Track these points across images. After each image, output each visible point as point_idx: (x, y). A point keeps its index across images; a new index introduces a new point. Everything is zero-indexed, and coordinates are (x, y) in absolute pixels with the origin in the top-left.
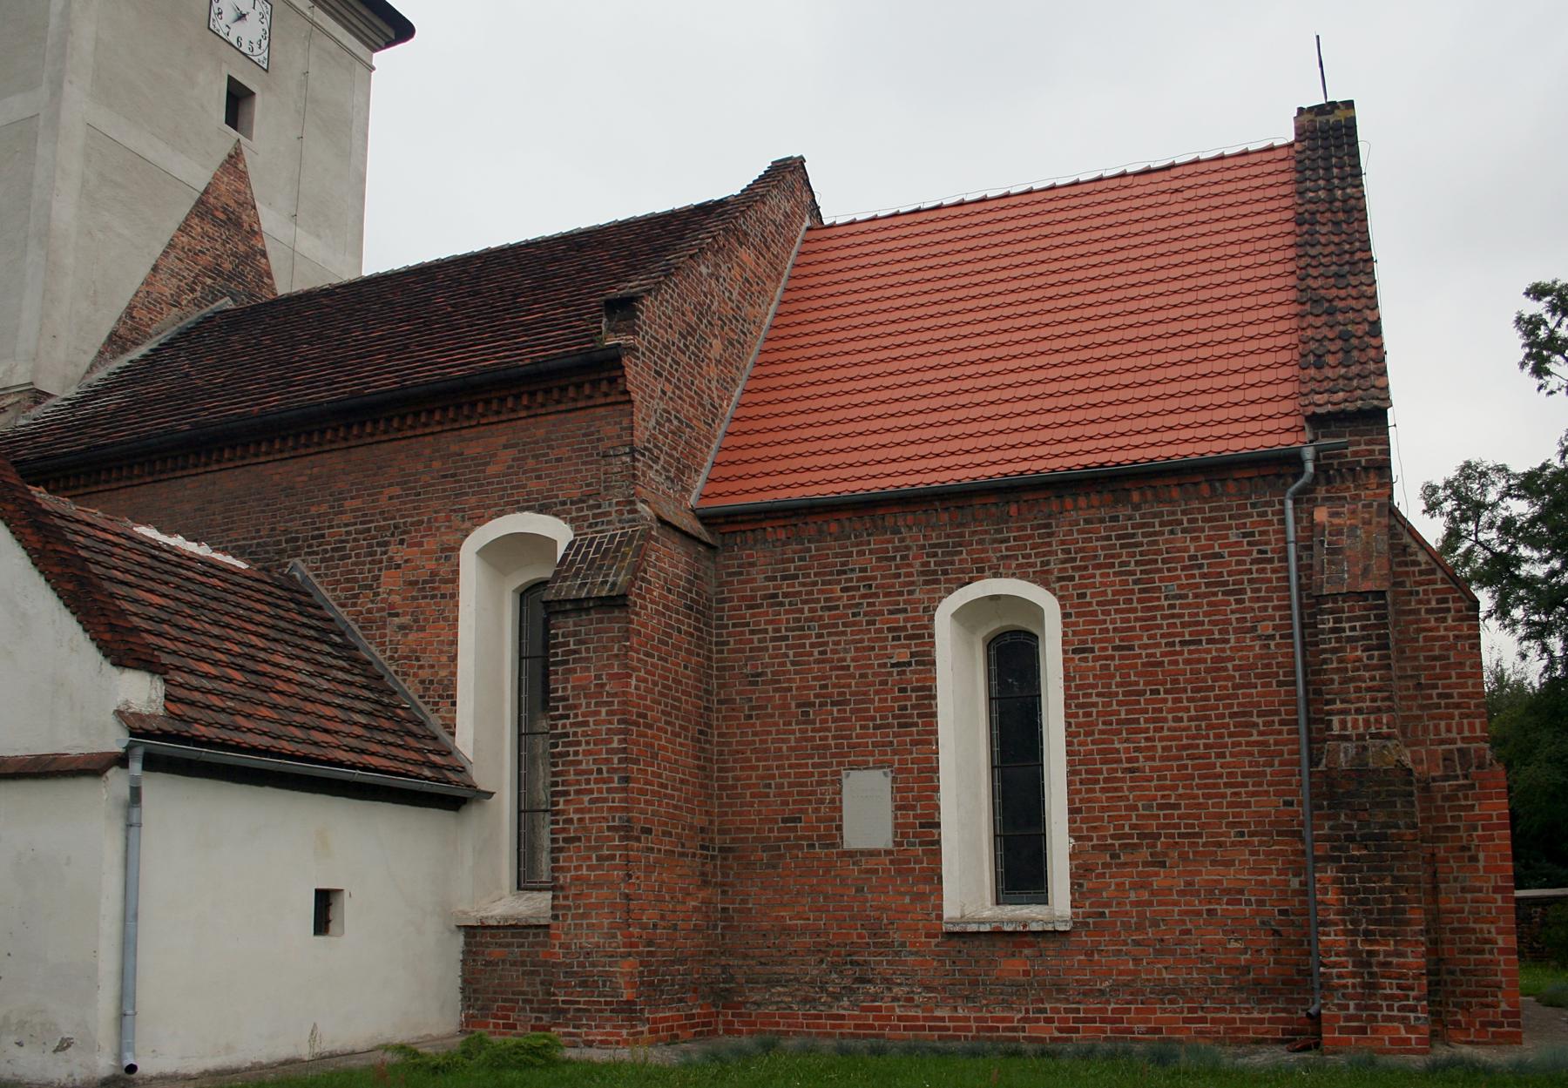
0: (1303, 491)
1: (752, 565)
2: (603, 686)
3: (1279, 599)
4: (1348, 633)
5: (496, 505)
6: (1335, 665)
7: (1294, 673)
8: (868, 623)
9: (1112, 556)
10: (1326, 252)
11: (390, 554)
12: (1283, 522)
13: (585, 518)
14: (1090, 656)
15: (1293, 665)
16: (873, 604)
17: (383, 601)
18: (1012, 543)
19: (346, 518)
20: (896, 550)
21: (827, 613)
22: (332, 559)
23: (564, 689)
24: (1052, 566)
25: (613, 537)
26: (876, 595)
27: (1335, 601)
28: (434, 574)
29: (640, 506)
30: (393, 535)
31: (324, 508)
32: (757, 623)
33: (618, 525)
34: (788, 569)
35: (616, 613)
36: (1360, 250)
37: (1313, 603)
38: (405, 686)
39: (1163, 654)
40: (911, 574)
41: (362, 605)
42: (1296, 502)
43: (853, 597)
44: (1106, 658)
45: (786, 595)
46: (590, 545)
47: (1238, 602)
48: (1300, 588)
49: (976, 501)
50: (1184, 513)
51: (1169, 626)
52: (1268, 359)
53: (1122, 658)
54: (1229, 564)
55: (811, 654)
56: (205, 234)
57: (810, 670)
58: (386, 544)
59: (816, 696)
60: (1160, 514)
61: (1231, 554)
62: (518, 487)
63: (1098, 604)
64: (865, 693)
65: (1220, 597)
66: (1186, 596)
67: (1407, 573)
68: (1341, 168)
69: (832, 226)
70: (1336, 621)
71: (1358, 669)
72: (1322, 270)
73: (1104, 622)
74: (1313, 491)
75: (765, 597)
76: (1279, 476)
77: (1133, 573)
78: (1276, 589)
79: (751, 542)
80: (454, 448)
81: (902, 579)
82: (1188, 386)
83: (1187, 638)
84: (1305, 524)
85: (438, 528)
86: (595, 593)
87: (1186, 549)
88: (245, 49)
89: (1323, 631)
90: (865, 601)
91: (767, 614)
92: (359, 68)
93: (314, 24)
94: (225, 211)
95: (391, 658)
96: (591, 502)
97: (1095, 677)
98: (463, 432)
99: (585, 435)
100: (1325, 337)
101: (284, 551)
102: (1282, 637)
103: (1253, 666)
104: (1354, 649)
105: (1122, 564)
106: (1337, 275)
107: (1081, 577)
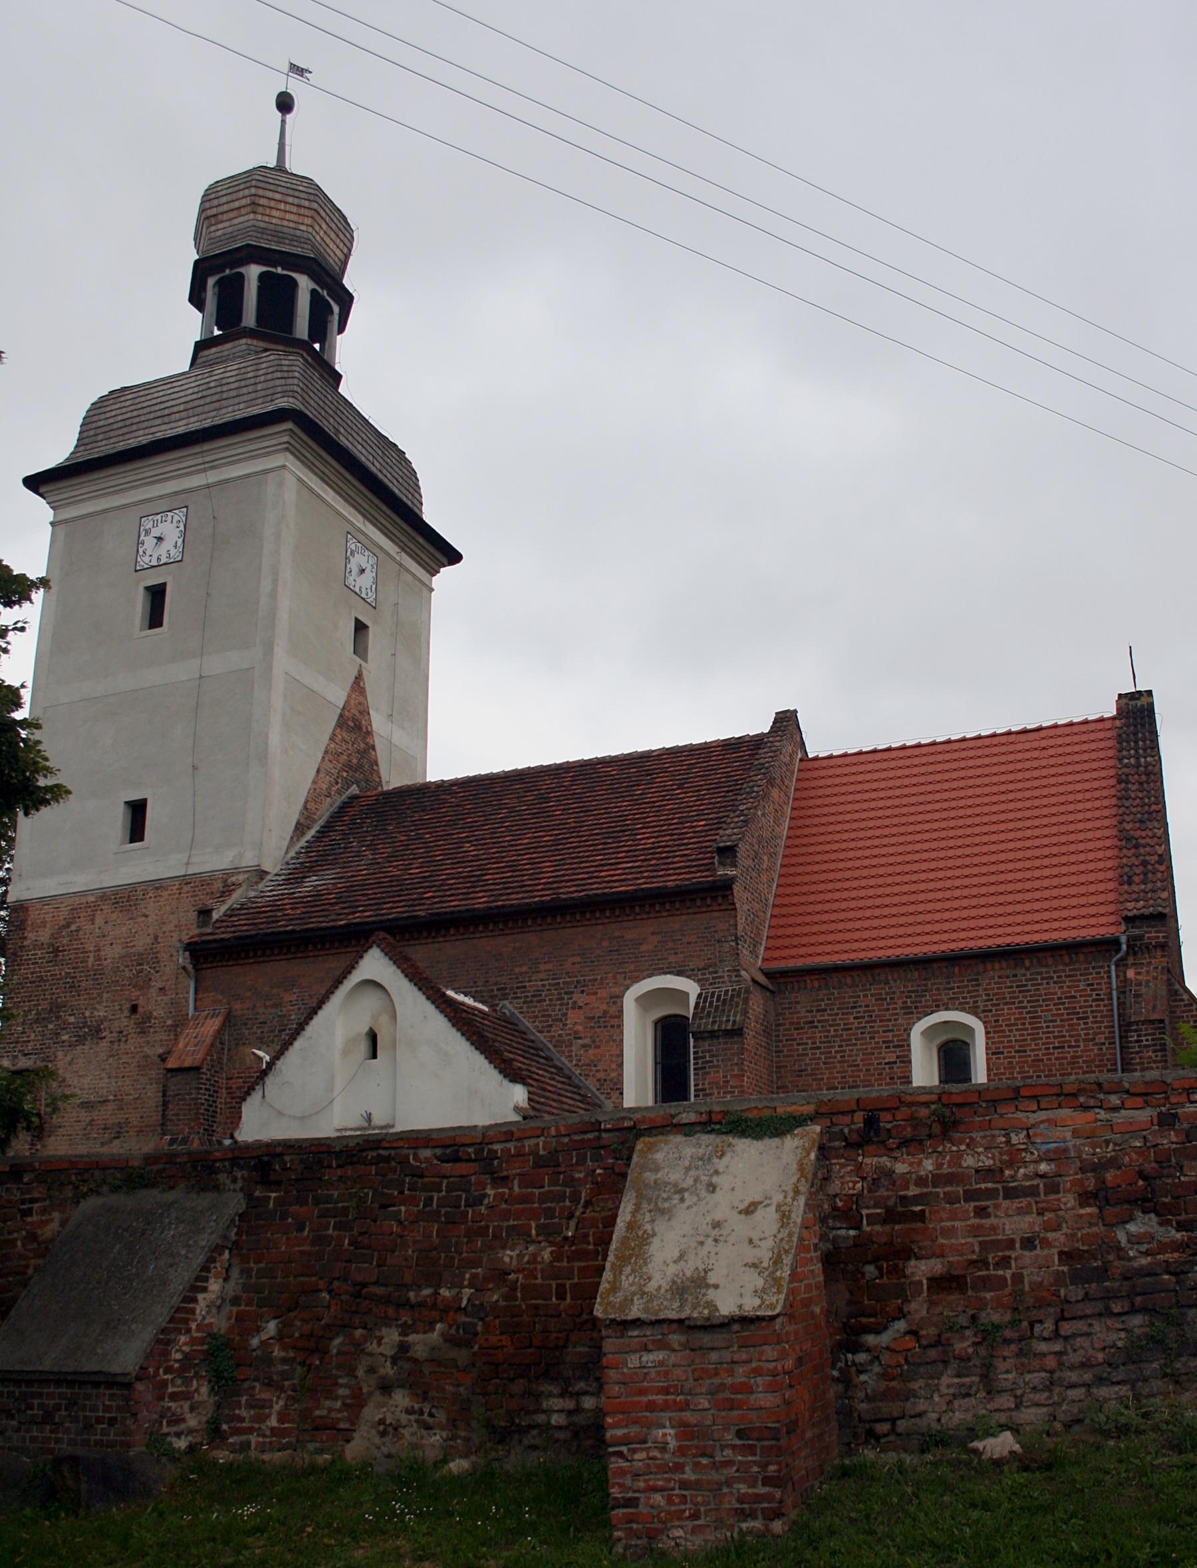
0: (1122, 959)
1: (798, 1003)
2: (728, 1082)
3: (1108, 1022)
4: (1145, 1043)
5: (647, 970)
6: (1138, 1061)
7: (1116, 1064)
8: (871, 1038)
9: (1014, 998)
10: (1135, 804)
11: (574, 999)
12: (1109, 977)
13: (707, 979)
14: (1002, 1056)
15: (1116, 1060)
16: (873, 1027)
17: (570, 1029)
18: (956, 990)
19: (541, 976)
20: (887, 994)
21: (845, 1032)
22: (532, 1001)
23: (703, 1084)
24: (979, 1004)
25: (727, 992)
26: (875, 1021)
27: (1137, 1025)
28: (605, 1012)
29: (743, 973)
30: (576, 987)
31: (524, 969)
32: (801, 1039)
33: (729, 984)
34: (821, 1005)
35: (736, 1039)
36: (1154, 803)
37: (1126, 1026)
38: (587, 1083)
39: (1043, 1055)
40: (896, 1009)
41: (555, 1031)
42: (1117, 966)
43: (861, 1023)
44: (1011, 1057)
45: (819, 1021)
46: (712, 996)
47: (1085, 1023)
48: (1119, 1015)
49: (935, 966)
50: (1054, 972)
51: (1046, 1038)
52: (1099, 834)
53: (1020, 1057)
54: (1080, 1002)
55: (835, 1057)
56: (343, 740)
57: (835, 1067)
58: (572, 993)
59: (839, 1083)
60: (1041, 973)
61: (1081, 996)
62: (661, 959)
63: (1006, 1025)
64: (869, 1081)
65: (1075, 1021)
66: (1055, 1021)
67: (1177, 1006)
68: (1144, 741)
69: (816, 759)
70: (1138, 1036)
71: (1150, 1063)
72: (1132, 817)
73: (1010, 1036)
74: (1126, 959)
75: (805, 1023)
76: (1107, 951)
77: (1025, 1007)
78: (1106, 1016)
79: (796, 988)
80: (617, 934)
81: (891, 1012)
82: (1055, 892)
83: (1057, 1045)
84: (1122, 978)
85: (608, 984)
86: (723, 1027)
87: (1056, 993)
88: (363, 595)
89: (1131, 1042)
90: (868, 1025)
91: (807, 1033)
92: (425, 591)
93: (401, 565)
94: (353, 720)
95: (576, 1065)
96: (711, 970)
97: (1005, 1068)
98: (624, 924)
99: (706, 928)
100: (1133, 864)
101: (496, 996)
102: (1109, 1044)
103: (1094, 1061)
104: (1148, 1051)
105: (1020, 1002)
106: (1141, 821)
107: (996, 1010)
